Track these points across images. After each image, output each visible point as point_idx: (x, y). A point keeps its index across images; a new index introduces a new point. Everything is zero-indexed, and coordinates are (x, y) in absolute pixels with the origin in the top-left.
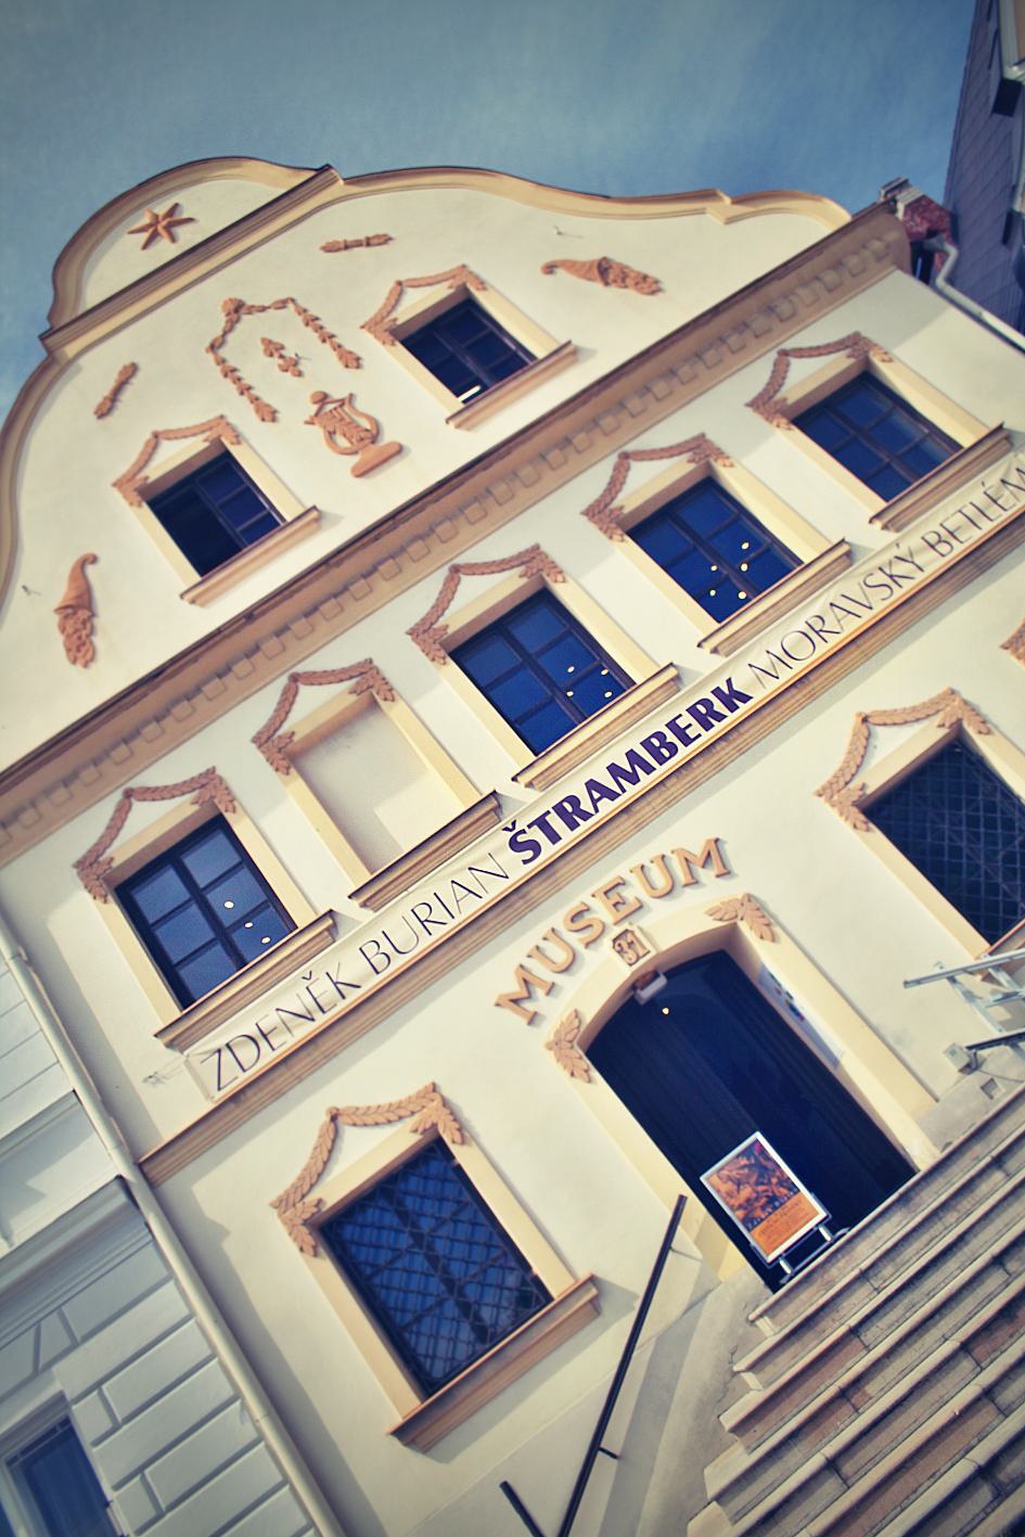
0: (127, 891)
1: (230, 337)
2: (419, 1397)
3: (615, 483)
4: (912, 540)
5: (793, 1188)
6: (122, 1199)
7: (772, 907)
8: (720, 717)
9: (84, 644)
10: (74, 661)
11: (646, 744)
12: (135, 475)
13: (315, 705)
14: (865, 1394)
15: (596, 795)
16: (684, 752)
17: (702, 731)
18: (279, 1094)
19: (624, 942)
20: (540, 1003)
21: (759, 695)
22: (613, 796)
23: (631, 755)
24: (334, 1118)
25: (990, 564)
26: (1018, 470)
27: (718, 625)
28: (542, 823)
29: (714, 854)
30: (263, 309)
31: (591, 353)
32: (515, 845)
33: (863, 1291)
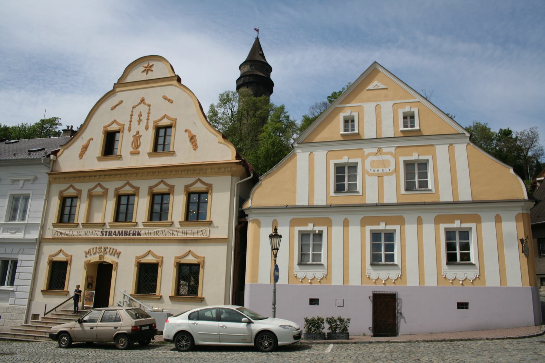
0: (189, 195)
1: (138, 107)
3: (157, 185)
4: (185, 229)
5: (93, 301)
6: (35, 241)
7: (119, 267)
9: (82, 155)
10: (79, 157)
11: (125, 231)
12: (157, 122)
13: (99, 190)
15: (114, 234)
16: (128, 236)
17: (132, 235)
18: (58, 242)
20: (88, 255)
21: (143, 236)
22: (116, 235)
24: (189, 252)
25: (186, 243)
26: (206, 231)
28: (106, 232)
29: (118, 254)
32: (102, 232)
33: (65, 316)
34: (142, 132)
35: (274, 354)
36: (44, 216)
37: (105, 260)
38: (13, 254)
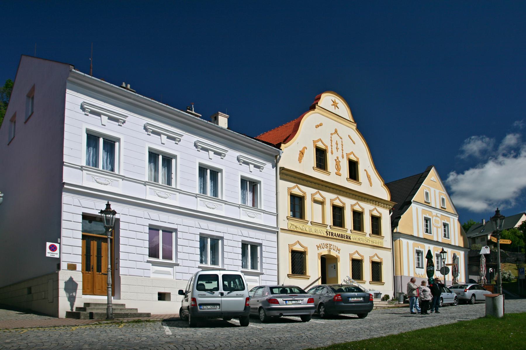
2: (334, 204)
8: (348, 239)
11: (341, 234)
14: (323, 302)
16: (343, 239)
19: (329, 251)
21: (352, 240)
22: (336, 237)
23: (340, 234)
27: (252, 207)
28: (330, 232)
30: (339, 136)
31: (360, 184)
32: (326, 232)
34: (340, 159)
35: (34, 344)
36: (121, 178)
37: (332, 254)
38: (200, 226)
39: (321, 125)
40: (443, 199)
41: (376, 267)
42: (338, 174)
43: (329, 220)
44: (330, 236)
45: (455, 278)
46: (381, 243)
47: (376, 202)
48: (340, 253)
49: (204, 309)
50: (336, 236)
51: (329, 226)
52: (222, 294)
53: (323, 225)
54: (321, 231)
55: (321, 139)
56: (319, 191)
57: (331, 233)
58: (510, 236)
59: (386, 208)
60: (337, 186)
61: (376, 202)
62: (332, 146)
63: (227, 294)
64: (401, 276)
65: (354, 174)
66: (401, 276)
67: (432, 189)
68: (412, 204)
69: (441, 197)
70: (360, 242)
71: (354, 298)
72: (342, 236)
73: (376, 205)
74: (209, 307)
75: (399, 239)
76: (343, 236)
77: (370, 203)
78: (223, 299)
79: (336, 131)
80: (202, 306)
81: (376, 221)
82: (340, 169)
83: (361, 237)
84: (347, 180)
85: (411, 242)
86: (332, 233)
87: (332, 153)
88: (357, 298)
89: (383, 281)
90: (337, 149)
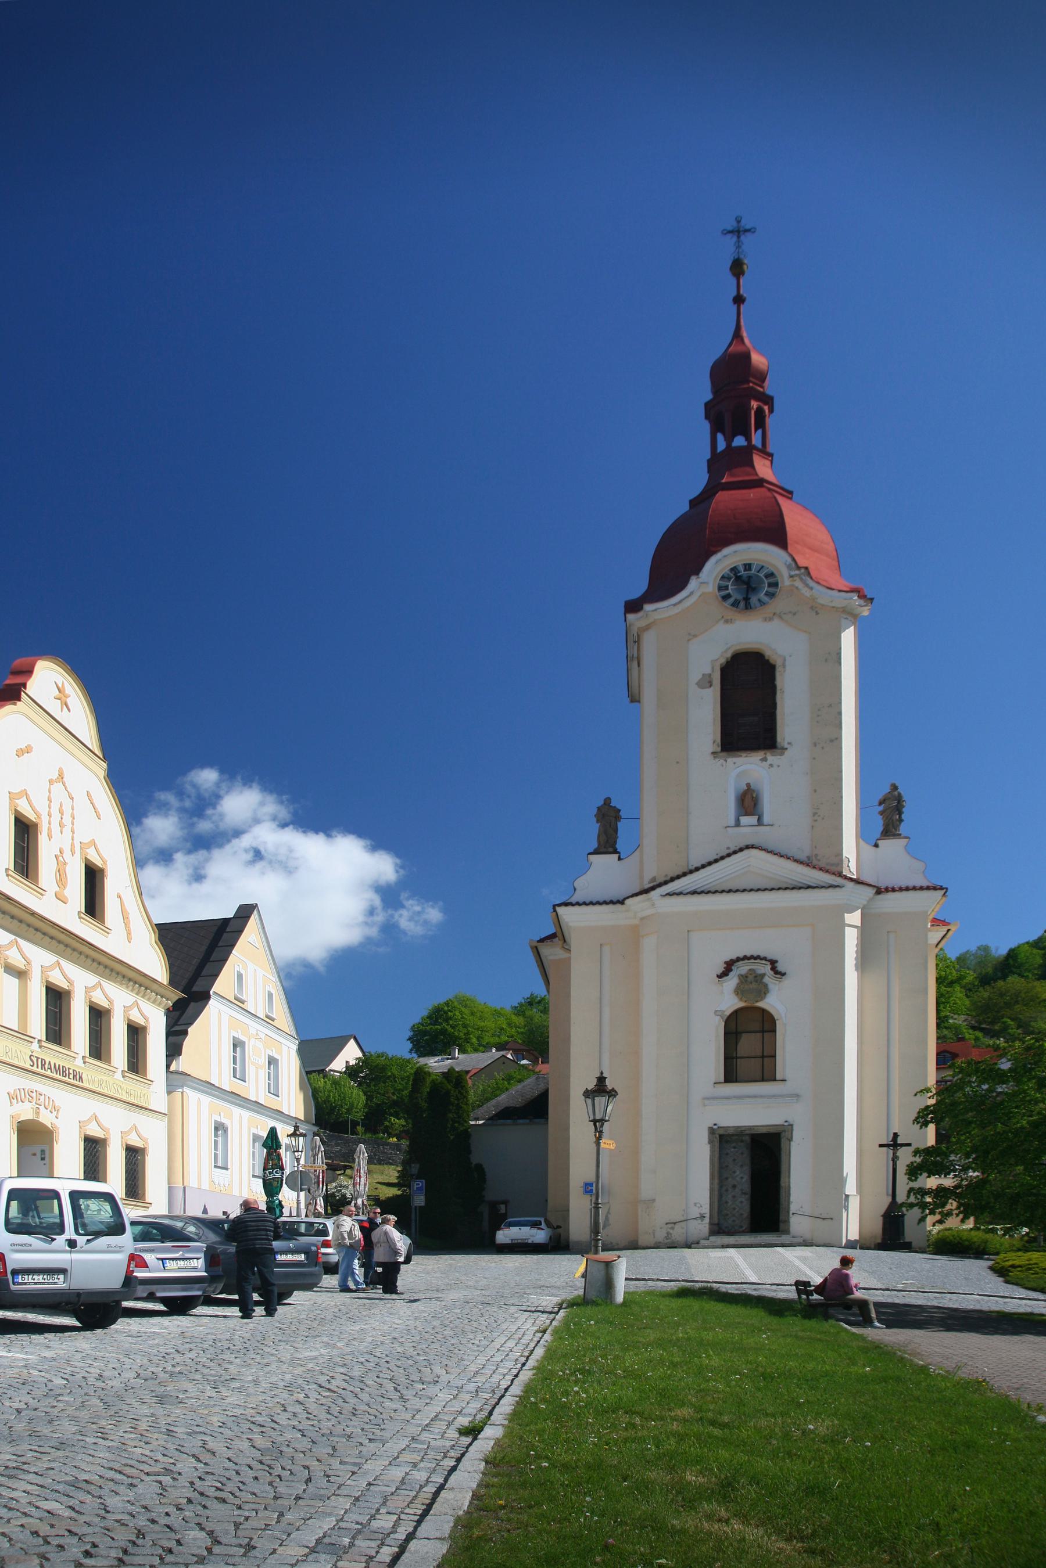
21: (85, 1085)
23: (59, 1065)
28: (38, 1058)
39: (28, 750)
40: (270, 995)
41: (134, 1156)
42: (61, 898)
43: (38, 1026)
44: (37, 1069)
45: (316, 1200)
46: (146, 1097)
47: (135, 983)
48: (59, 1117)
49: (25, 1284)
50: (50, 1068)
51: (37, 1040)
52: (72, 1244)
53: (22, 1034)
54: (19, 1052)
55: (28, 792)
56: (19, 940)
57: (40, 1060)
58: (329, 1092)
59: (159, 1005)
60: (63, 932)
61: (135, 983)
62: (50, 815)
63: (86, 1244)
64: (184, 1188)
65: (93, 906)
66: (184, 1188)
67: (251, 966)
68: (211, 1002)
69: (267, 989)
70: (118, 1096)
71: (286, 1255)
72: (63, 1071)
73: (137, 994)
74: (38, 1278)
75: (180, 1090)
76: (67, 1072)
77: (127, 987)
78: (75, 1256)
79: (61, 776)
80: (20, 1277)
81: (136, 1033)
82: (66, 883)
83: (105, 1078)
84: (80, 918)
85: (206, 1100)
86: (42, 1060)
87: (50, 837)
88: (292, 1255)
89: (148, 1199)
90: (61, 825)
